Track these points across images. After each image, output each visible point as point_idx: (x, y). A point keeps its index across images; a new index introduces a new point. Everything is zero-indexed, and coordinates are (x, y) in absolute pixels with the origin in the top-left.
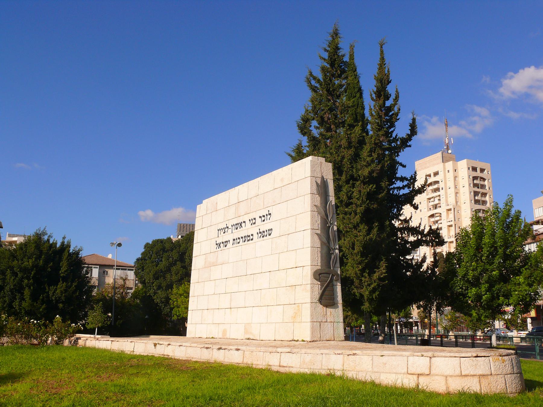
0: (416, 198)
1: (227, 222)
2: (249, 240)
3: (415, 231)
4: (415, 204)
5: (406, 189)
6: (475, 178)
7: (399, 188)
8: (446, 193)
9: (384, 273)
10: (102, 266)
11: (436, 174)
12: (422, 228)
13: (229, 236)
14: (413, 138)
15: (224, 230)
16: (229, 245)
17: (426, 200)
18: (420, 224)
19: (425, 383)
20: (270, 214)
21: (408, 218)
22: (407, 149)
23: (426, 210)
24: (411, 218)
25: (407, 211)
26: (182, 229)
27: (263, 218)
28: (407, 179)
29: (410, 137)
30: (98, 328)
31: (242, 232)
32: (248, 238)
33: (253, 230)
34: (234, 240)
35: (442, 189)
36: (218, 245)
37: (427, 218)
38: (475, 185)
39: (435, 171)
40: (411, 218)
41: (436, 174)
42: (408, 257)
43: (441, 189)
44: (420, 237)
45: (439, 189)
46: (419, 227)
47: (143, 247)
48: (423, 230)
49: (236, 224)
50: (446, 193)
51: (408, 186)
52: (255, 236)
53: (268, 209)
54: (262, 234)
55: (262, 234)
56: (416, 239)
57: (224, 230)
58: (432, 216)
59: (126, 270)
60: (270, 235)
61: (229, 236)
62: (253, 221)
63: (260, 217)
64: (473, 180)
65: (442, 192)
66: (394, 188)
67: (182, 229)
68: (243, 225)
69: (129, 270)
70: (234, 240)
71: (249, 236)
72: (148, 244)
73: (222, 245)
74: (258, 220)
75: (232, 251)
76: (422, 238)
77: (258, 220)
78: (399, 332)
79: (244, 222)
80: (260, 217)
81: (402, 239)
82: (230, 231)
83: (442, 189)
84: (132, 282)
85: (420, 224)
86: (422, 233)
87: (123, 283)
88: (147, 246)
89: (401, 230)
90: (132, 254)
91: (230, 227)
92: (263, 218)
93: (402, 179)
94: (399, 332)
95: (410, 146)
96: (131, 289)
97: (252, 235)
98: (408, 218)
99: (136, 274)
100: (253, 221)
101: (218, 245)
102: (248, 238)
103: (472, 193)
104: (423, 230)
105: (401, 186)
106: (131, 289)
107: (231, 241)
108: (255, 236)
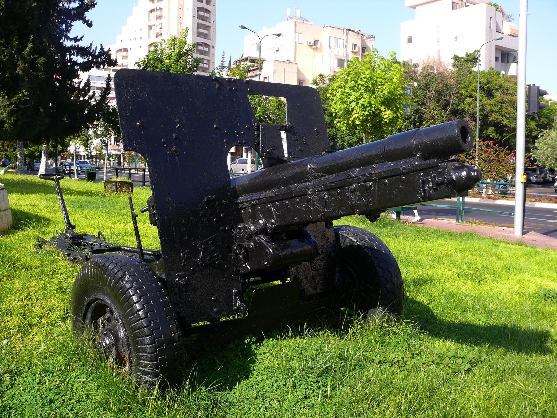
3: (84, 52)
4: (89, 20)
6: (200, 9)
8: (169, 22)
9: (26, 96)
12: (93, 48)
18: (91, 44)
19: (19, 196)
21: (79, 38)
25: (77, 28)
38: (199, 17)
39: (406, 40)
40: (81, 38)
43: (163, 17)
45: (162, 16)
46: (90, 47)
50: (169, 22)
56: (86, 60)
64: (198, 11)
76: (92, 59)
78: (259, 278)
85: (91, 44)
86: (93, 55)
94: (259, 278)
98: (79, 38)
103: (196, 25)
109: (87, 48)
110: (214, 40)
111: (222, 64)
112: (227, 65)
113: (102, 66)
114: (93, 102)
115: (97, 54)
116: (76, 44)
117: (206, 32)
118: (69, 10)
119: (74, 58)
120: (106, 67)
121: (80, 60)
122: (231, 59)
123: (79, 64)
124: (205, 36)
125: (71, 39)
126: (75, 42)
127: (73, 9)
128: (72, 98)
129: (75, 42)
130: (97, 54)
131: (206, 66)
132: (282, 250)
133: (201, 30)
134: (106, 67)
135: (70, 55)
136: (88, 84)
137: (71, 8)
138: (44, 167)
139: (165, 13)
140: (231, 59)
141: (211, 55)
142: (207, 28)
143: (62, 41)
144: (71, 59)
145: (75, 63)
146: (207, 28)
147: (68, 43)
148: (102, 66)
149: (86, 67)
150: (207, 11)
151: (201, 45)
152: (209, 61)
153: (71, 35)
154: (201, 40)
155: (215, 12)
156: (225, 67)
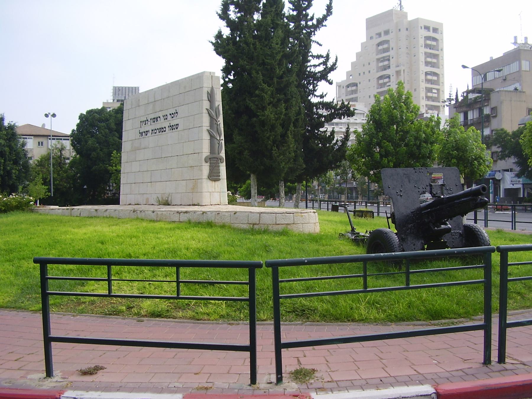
0: (329, 75)
1: (147, 116)
2: (162, 132)
3: (327, 106)
5: (322, 66)
7: (315, 66)
10: (274, 266)
11: (387, 32)
13: (149, 127)
14: (328, 18)
15: (145, 122)
16: (149, 134)
17: (375, 60)
18: (334, 100)
20: (177, 113)
22: (322, 29)
23: (375, 71)
24: (325, 95)
26: (117, 92)
27: (172, 116)
28: (322, 57)
29: (325, 18)
30: (40, 199)
31: (158, 125)
32: (162, 130)
33: (166, 124)
34: (152, 130)
35: (392, 49)
36: (141, 134)
37: (376, 80)
39: (386, 28)
40: (325, 95)
41: (387, 32)
42: (321, 129)
44: (333, 111)
46: (333, 102)
47: (78, 118)
48: (337, 105)
49: (154, 118)
51: (325, 63)
52: (167, 129)
53: (176, 108)
54: (172, 127)
55: (172, 127)
56: (330, 113)
57: (145, 122)
58: (381, 78)
59: (61, 139)
60: (177, 128)
61: (149, 127)
62: (165, 117)
63: (170, 114)
64: (425, 41)
65: (391, 53)
66: (311, 66)
67: (117, 92)
68: (159, 119)
69: (64, 139)
70: (152, 130)
71: (163, 128)
72: (82, 114)
73: (143, 134)
74: (169, 117)
75: (151, 140)
77: (169, 117)
79: (159, 117)
80: (170, 114)
81: (317, 113)
82: (149, 123)
83: (392, 49)
84: (68, 152)
86: (334, 108)
87: (59, 154)
88: (82, 117)
89: (317, 105)
90: (68, 125)
91: (149, 120)
92: (172, 116)
93: (318, 57)
95: (325, 26)
96: (68, 159)
97: (165, 128)
99: (73, 145)
100: (165, 117)
101: (141, 134)
102: (162, 130)
104: (337, 105)
105: (317, 64)
106: (68, 159)
107: (151, 131)
108: (167, 129)
109: (330, 102)
110: (443, 68)
111: (450, 96)
112: (454, 97)
113: (343, 117)
114: (336, 147)
115: (338, 107)
116: (322, 100)
117: (434, 61)
118: (315, 74)
119: (320, 112)
120: (346, 117)
121: (324, 112)
122: (457, 93)
123: (325, 116)
124: (433, 65)
125: (317, 96)
126: (321, 98)
127: (319, 72)
128: (309, 129)
129: (321, 98)
130: (338, 107)
131: (436, 95)
132: (40, 204)
133: (429, 60)
134: (346, 117)
135: (317, 109)
136: (333, 133)
137: (317, 71)
138: (469, 323)
139: (392, 44)
140: (457, 93)
141: (441, 84)
142: (436, 56)
143: (309, 98)
144: (318, 113)
145: (321, 116)
146: (436, 56)
147: (314, 100)
148: (343, 117)
149: (329, 119)
150: (435, 39)
151: (429, 74)
152: (438, 90)
153: (317, 93)
154: (429, 69)
155: (442, 40)
156: (453, 100)
